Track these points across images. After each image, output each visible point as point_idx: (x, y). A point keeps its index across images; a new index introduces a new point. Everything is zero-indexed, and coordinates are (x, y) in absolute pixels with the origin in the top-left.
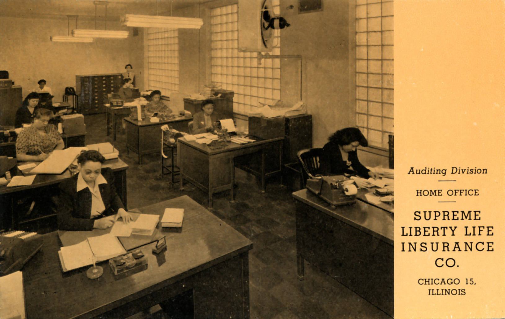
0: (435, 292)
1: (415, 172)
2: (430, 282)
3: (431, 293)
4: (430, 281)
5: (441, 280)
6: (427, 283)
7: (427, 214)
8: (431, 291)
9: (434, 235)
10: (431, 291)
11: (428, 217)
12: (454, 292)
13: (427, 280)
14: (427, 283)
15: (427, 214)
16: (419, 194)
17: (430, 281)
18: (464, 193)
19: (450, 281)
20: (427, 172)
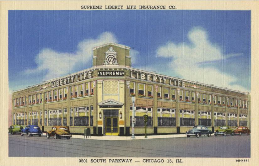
0: (179, 161)
1: (115, 161)
2: (149, 161)
3: (177, 161)
4: (149, 160)
5: (154, 160)
6: (147, 161)
7: (148, 7)
8: (178, 160)
9: (103, 162)
10: (178, 160)
11: (85, 8)
12: (95, 161)
13: (147, 160)
14: (147, 161)
15: (148, 7)
16: (147, 160)
17: (149, 160)
18: (102, 161)
19: (159, 161)
20: (87, 7)
